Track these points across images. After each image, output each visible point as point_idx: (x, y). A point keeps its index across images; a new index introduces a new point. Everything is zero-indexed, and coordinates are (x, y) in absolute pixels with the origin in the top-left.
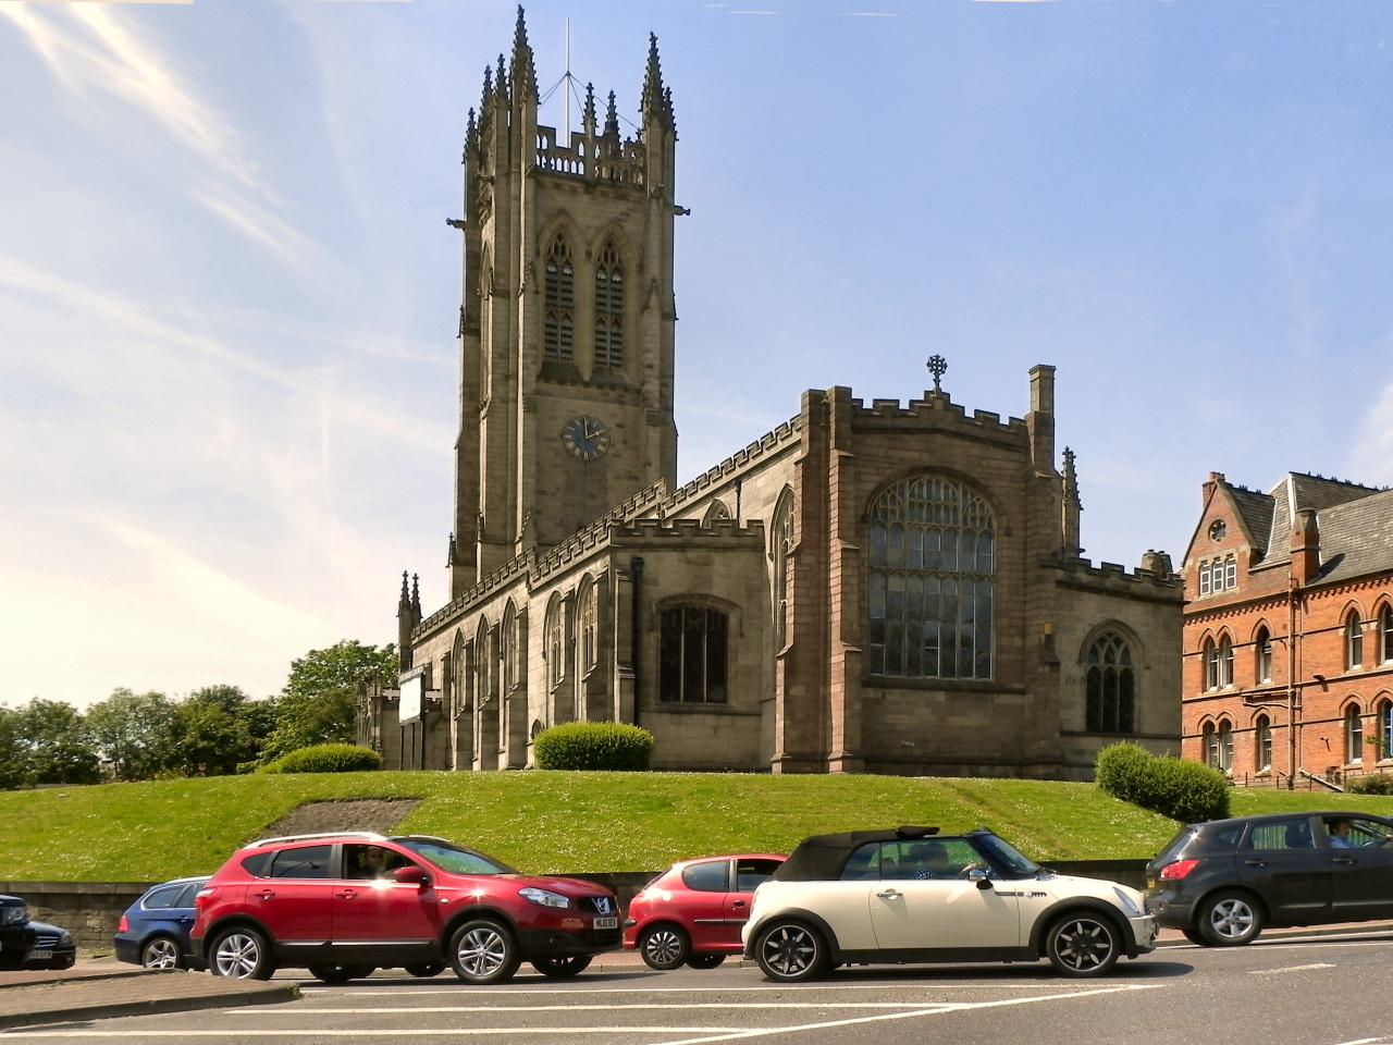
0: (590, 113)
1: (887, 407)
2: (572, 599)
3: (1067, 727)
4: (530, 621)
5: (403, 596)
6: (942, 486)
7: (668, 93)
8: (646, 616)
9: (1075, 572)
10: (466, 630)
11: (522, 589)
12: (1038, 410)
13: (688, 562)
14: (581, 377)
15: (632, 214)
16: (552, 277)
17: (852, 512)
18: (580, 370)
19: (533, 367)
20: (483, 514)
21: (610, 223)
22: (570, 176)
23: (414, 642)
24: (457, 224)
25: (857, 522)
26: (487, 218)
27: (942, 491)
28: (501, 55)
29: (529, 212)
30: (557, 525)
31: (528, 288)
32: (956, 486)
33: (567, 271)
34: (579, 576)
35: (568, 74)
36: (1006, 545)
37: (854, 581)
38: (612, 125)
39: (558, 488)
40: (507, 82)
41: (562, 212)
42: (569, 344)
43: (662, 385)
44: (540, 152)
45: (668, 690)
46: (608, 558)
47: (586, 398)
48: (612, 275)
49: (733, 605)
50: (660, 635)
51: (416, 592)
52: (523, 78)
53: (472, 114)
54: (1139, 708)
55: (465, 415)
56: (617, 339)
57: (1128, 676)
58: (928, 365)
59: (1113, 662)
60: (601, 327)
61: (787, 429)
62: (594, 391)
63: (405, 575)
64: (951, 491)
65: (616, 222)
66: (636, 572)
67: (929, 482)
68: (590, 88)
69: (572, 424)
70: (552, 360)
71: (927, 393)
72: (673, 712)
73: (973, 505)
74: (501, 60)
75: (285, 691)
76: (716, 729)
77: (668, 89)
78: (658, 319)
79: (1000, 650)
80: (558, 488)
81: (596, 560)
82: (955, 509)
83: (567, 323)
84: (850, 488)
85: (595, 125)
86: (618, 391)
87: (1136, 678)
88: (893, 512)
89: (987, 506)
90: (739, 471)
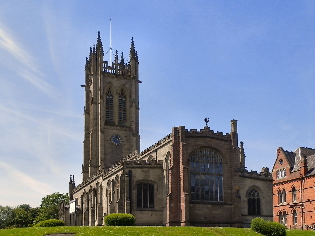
2: (113, 181)
3: (243, 214)
7: (137, 52)
8: (133, 186)
11: (101, 179)
12: (233, 131)
13: (143, 171)
15: (128, 83)
16: (108, 99)
18: (115, 122)
20: (91, 160)
21: (122, 85)
23: (73, 193)
26: (91, 84)
30: (109, 162)
32: (213, 151)
33: (111, 97)
34: (115, 175)
35: (111, 48)
37: (187, 176)
38: (122, 61)
39: (110, 153)
40: (96, 50)
41: (110, 82)
44: (104, 68)
45: (139, 205)
46: (123, 170)
47: (117, 129)
48: (123, 98)
49: (155, 183)
51: (74, 180)
53: (87, 58)
55: (86, 134)
57: (259, 200)
58: (205, 120)
59: (255, 197)
60: (120, 112)
61: (168, 137)
62: (118, 128)
65: (124, 85)
67: (206, 150)
68: (117, 52)
74: (94, 45)
75: (40, 205)
76: (151, 215)
77: (136, 51)
79: (225, 194)
82: (212, 157)
83: (111, 111)
87: (261, 201)
88: (196, 158)
89: (221, 156)
90: (156, 148)
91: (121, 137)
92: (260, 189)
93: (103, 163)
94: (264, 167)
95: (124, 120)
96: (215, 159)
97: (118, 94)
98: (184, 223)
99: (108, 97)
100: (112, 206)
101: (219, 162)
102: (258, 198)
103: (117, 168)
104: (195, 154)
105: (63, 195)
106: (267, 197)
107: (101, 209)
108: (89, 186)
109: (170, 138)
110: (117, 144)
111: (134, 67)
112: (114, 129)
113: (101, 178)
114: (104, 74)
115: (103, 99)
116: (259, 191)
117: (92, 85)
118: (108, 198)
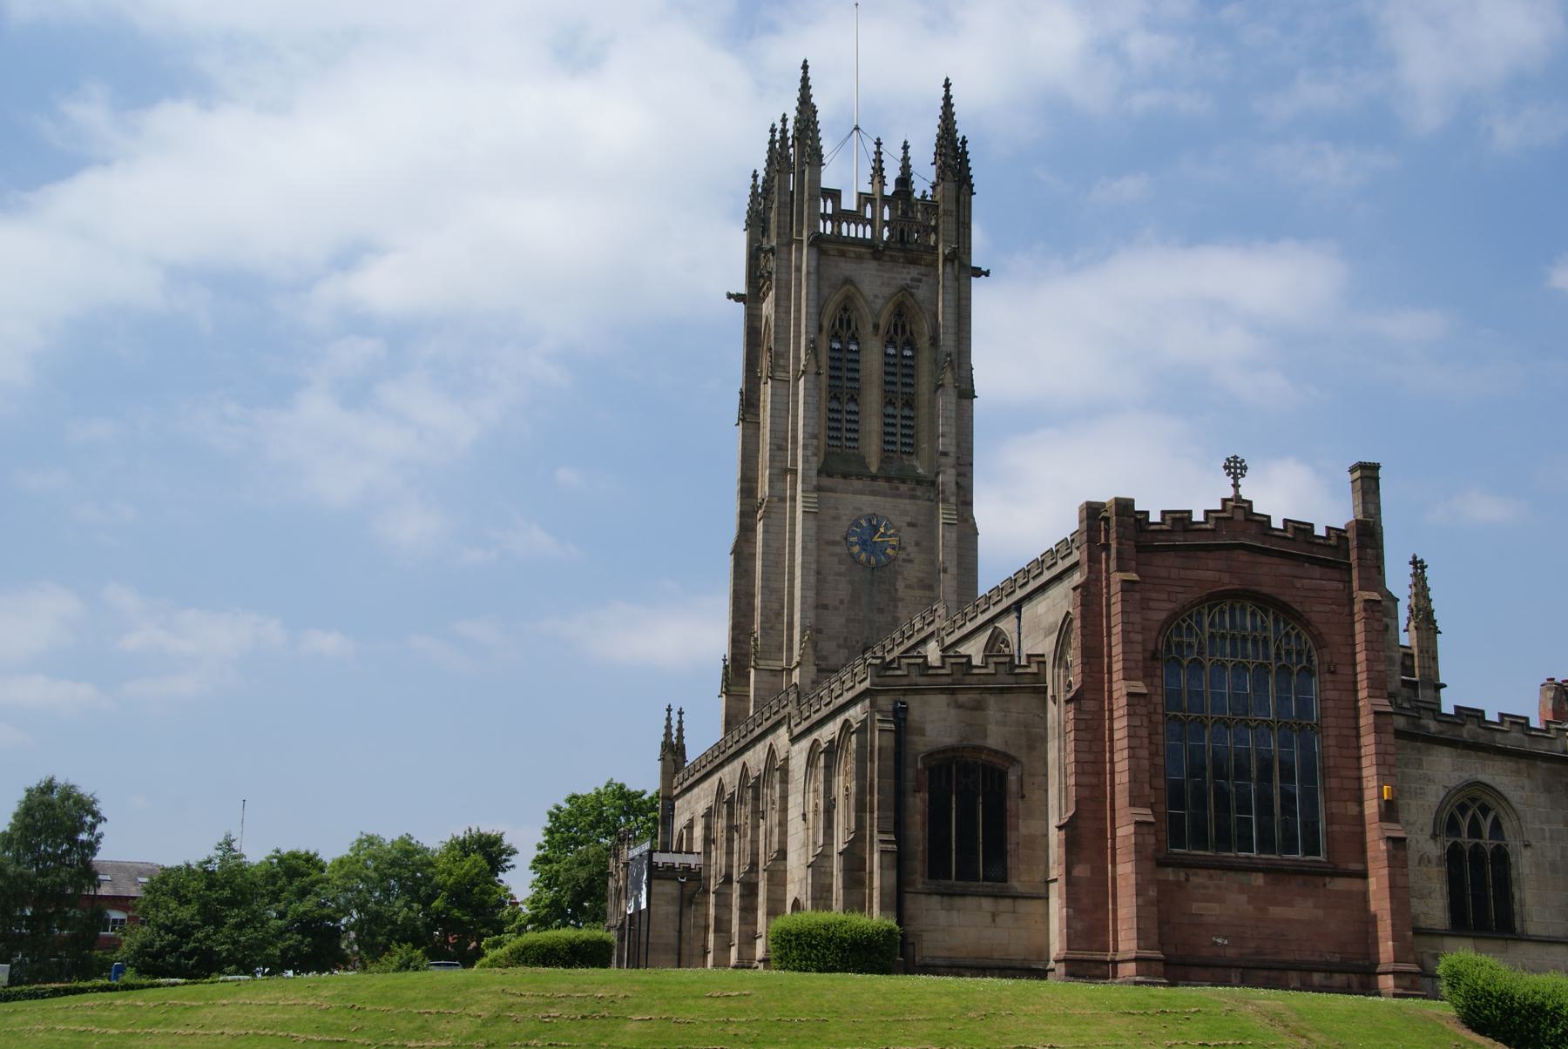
0: (878, 171)
1: (1180, 520)
2: (832, 751)
3: (1424, 923)
4: (790, 774)
5: (665, 735)
6: (1249, 611)
7: (964, 142)
8: (910, 773)
9: (1420, 718)
10: (728, 781)
11: (783, 734)
12: (1360, 517)
13: (959, 706)
14: (867, 468)
15: (924, 278)
16: (837, 355)
17: (1139, 648)
18: (867, 460)
19: (814, 459)
20: (758, 634)
21: (901, 290)
22: (856, 242)
23: (675, 792)
24: (738, 298)
25: (1144, 659)
26: (769, 289)
27: (1248, 617)
28: (784, 115)
29: (811, 295)
30: (839, 646)
31: (809, 368)
32: (1266, 612)
33: (853, 347)
34: (839, 721)
35: (857, 128)
36: (1329, 686)
37: (1144, 733)
38: (904, 181)
39: (842, 602)
40: (790, 143)
41: (848, 281)
42: (856, 431)
43: (959, 475)
44: (825, 217)
45: (937, 867)
46: (867, 702)
47: (874, 493)
48: (903, 349)
49: (1012, 760)
50: (927, 796)
51: (680, 730)
52: (807, 137)
53: (755, 176)
54: (1520, 900)
55: (743, 514)
56: (908, 422)
57: (1502, 858)
58: (1225, 467)
59: (1480, 837)
60: (890, 410)
61: (1066, 545)
62: (881, 484)
63: (669, 710)
64: (1259, 618)
65: (906, 290)
66: (900, 715)
67: (1232, 609)
68: (879, 144)
69: (857, 523)
70: (835, 449)
71: (1224, 501)
72: (942, 895)
73: (1287, 634)
74: (784, 120)
75: (540, 847)
76: (994, 916)
77: (964, 137)
78: (954, 399)
79: (1330, 820)
80: (842, 602)
81: (856, 704)
82: (1266, 641)
83: (852, 407)
84: (1136, 618)
85: (883, 183)
86: (910, 485)
87: (1512, 860)
88: (1190, 646)
89: (1305, 636)
90: (1019, 594)
91: (894, 527)
92: (1506, 799)
93: (810, 651)
94: (1553, 679)
95: (904, 449)
96: (1278, 648)
97: (881, 331)
98: (1132, 966)
99: (836, 346)
100: (823, 869)
101: (1298, 664)
102: (1498, 846)
103: (845, 688)
104: (1185, 625)
105: (641, 795)
106: (1544, 839)
107: (778, 878)
108: (737, 765)
109: (1075, 551)
110: (873, 560)
111: (953, 208)
112: (862, 493)
113: (783, 732)
114: (824, 245)
115: (816, 356)
116: (1502, 813)
117: (772, 294)
118: (811, 826)
